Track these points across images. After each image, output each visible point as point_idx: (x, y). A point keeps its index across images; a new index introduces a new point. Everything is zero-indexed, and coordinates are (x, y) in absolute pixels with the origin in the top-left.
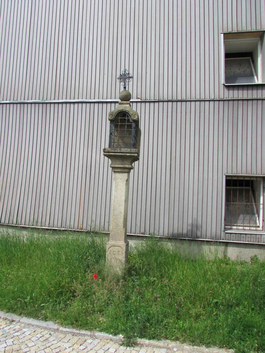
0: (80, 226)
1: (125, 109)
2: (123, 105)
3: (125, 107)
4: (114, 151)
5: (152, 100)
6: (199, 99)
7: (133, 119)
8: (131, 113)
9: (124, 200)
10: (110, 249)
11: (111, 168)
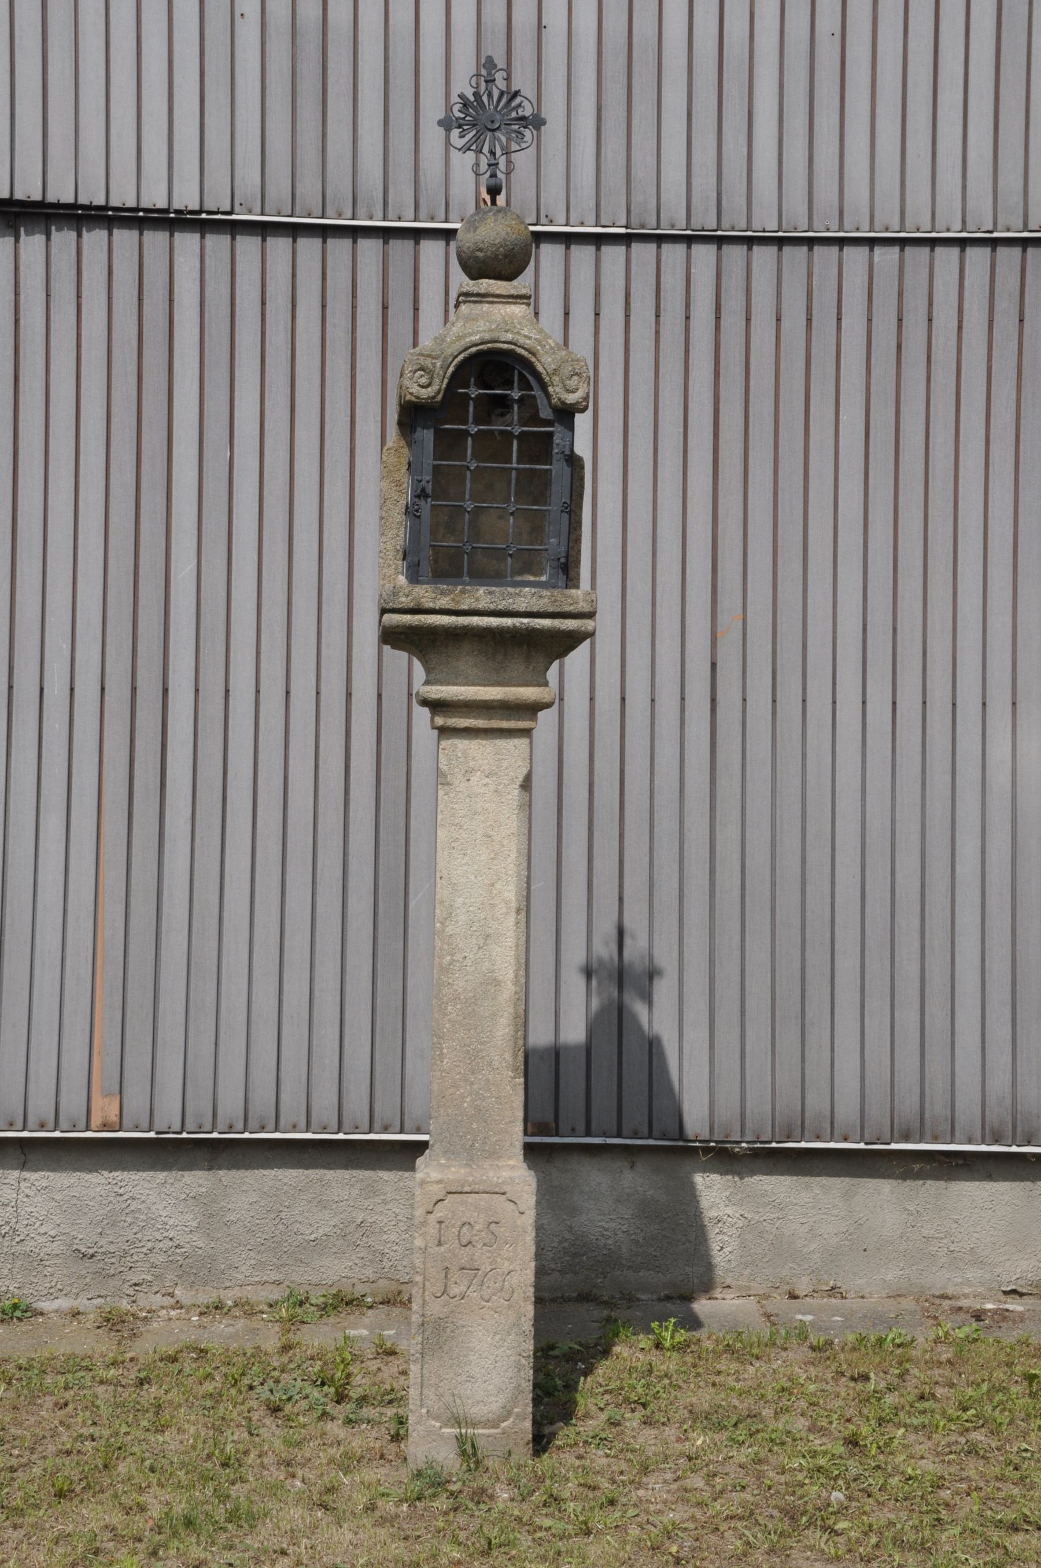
0: (105, 1108)
1: (509, 336)
2: (486, 307)
3: (507, 325)
4: (451, 606)
5: (795, 230)
6: (744, 226)
7: (563, 403)
8: (545, 363)
9: (514, 905)
10: (440, 1212)
11: (436, 732)
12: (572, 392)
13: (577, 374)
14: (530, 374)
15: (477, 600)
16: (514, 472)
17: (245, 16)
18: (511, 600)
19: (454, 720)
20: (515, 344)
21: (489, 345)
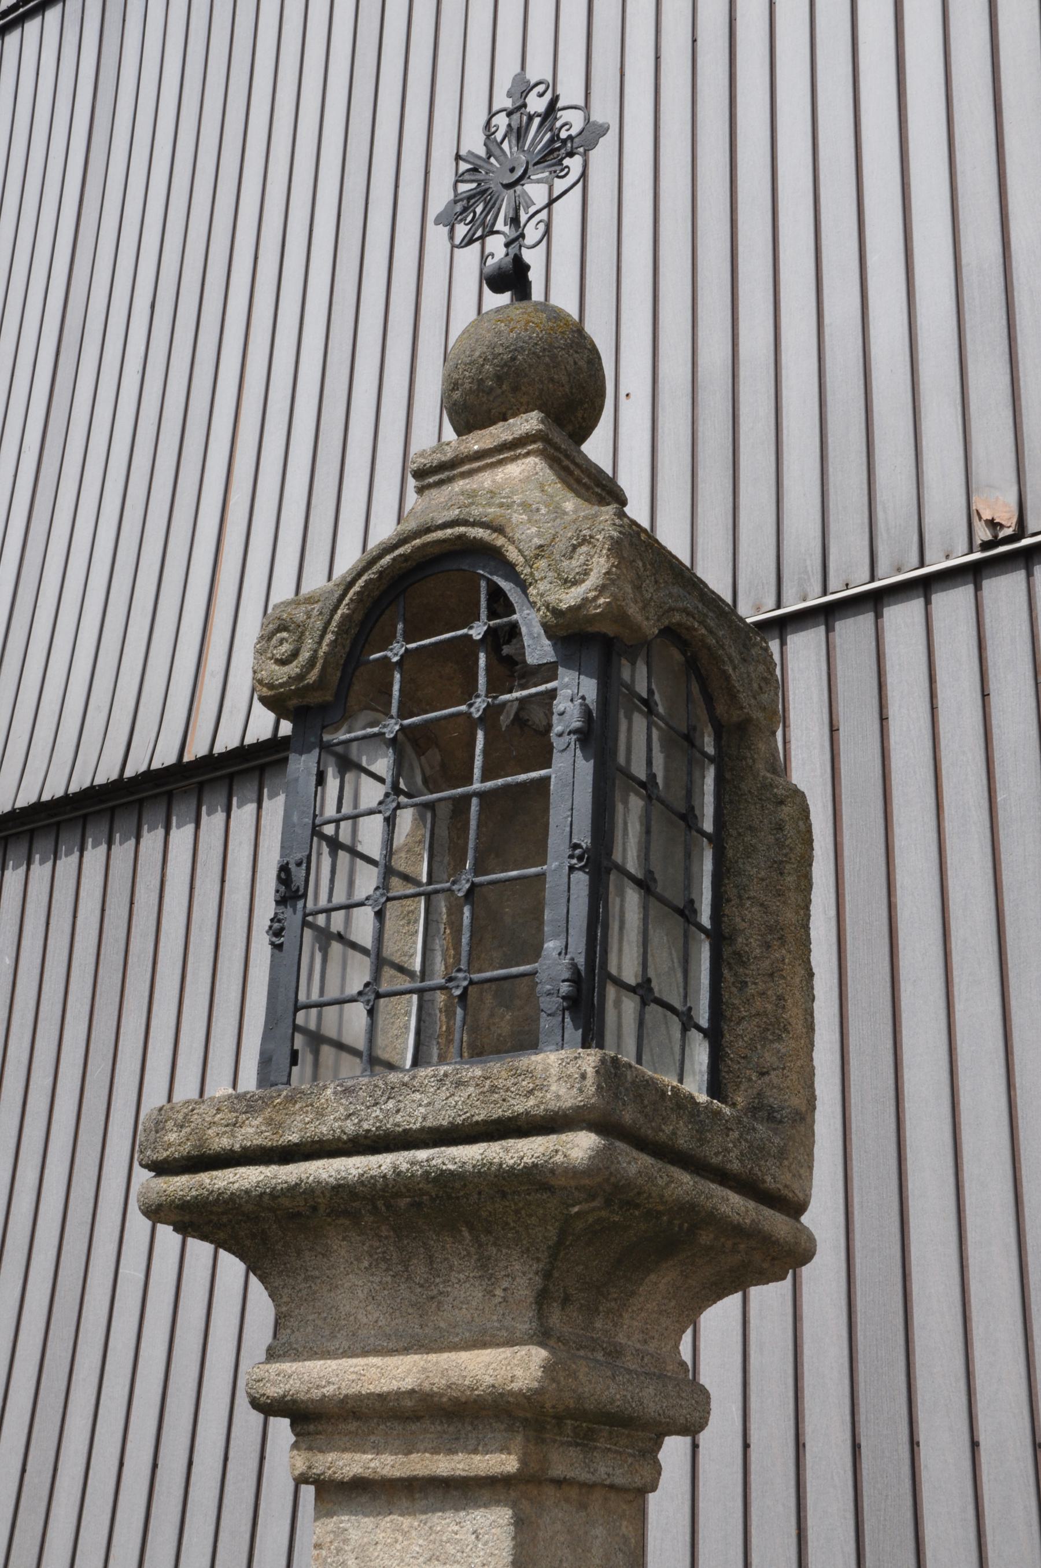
12: (575, 583)
13: (584, 541)
14: (507, 578)
15: (320, 1114)
16: (475, 801)
17: (632, 396)
18: (391, 1104)
19: (331, 1457)
20: (465, 523)
21: (417, 542)
